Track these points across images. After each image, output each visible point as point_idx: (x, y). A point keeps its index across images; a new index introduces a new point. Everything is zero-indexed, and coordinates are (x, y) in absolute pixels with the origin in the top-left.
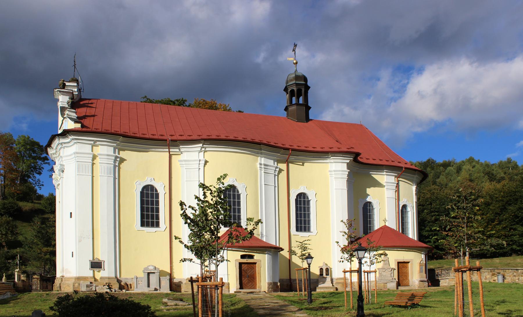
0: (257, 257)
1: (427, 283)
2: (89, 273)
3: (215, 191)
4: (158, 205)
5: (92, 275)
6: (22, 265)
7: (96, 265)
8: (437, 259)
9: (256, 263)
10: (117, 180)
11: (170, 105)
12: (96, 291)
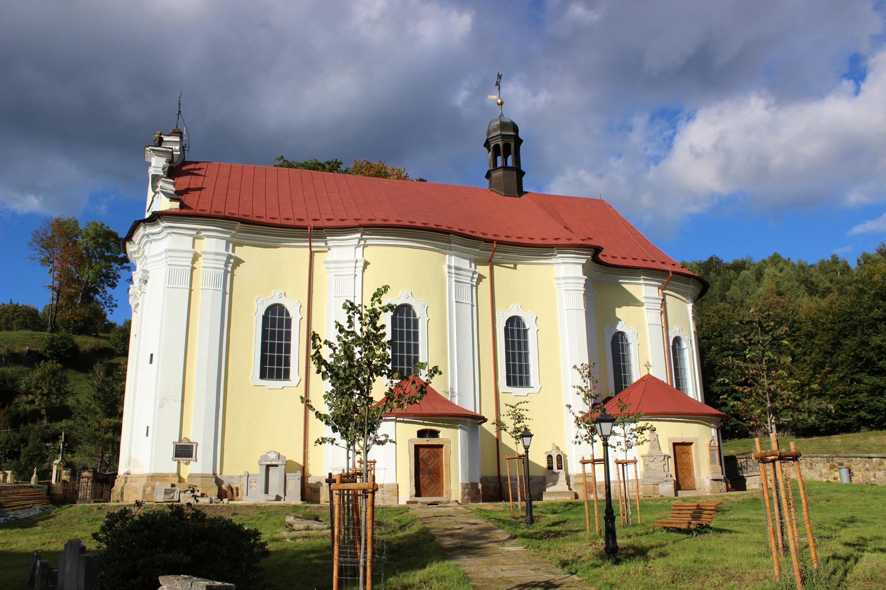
0: (445, 433)
1: (724, 484)
2: (169, 466)
3: (366, 315)
4: (290, 340)
5: (175, 471)
6: (67, 452)
7: (184, 451)
8: (740, 437)
9: (441, 446)
10: (228, 296)
11: (318, 170)
12: (179, 501)
